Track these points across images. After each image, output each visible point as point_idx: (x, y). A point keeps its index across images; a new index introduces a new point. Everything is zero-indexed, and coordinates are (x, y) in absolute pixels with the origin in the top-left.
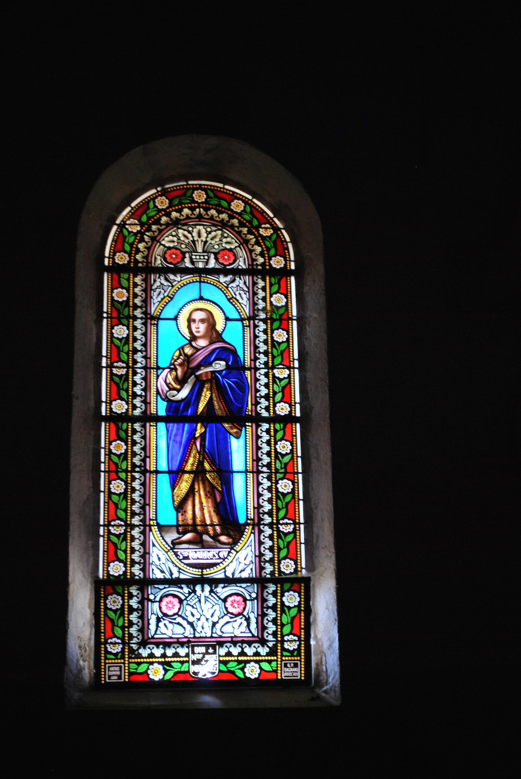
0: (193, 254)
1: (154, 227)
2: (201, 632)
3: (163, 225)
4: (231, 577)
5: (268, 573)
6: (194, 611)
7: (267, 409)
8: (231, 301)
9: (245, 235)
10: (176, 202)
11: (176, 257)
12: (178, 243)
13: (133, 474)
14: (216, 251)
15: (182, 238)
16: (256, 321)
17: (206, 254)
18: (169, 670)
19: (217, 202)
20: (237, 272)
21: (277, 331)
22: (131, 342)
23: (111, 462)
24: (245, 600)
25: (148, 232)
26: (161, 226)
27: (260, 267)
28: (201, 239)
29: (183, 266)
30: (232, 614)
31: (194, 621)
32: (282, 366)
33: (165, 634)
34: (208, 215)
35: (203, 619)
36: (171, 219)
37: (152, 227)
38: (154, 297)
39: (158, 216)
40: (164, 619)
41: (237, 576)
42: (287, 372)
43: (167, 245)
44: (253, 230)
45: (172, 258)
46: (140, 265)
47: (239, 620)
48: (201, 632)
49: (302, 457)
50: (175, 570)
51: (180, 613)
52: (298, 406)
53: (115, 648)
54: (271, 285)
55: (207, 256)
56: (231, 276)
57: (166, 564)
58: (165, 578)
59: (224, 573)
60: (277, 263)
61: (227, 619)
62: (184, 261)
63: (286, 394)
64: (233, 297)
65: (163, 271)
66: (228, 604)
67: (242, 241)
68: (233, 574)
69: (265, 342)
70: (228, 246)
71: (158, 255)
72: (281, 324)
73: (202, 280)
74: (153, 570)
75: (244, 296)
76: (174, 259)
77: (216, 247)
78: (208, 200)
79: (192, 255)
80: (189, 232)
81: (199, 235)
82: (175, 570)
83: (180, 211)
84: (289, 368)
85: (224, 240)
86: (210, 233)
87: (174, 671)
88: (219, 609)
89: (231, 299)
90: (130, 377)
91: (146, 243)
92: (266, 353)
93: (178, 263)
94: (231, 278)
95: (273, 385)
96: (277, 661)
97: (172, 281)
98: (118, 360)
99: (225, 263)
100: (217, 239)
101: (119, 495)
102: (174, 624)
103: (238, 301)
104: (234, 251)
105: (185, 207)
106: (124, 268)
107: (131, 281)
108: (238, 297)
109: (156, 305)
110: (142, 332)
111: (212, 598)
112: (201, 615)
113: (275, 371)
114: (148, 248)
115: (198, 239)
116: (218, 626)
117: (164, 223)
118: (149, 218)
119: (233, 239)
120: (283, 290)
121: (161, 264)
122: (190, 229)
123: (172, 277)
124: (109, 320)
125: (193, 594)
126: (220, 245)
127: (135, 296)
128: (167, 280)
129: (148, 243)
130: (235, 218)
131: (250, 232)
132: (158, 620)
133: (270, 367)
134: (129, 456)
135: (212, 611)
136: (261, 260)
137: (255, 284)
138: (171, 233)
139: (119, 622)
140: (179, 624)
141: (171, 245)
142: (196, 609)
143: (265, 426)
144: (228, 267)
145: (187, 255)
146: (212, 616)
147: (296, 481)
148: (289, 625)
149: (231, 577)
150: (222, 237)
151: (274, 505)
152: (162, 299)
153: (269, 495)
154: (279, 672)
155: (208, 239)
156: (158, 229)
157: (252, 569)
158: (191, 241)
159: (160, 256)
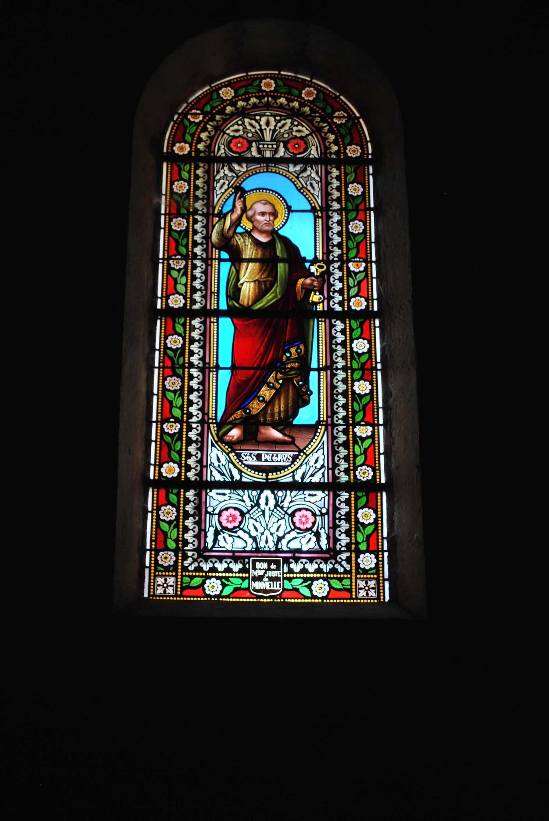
0: (260, 143)
1: (218, 117)
2: (265, 547)
3: (228, 114)
4: (300, 481)
5: (336, 256)
6: (258, 525)
7: (341, 303)
8: (302, 191)
9: (317, 124)
10: (242, 91)
11: (242, 146)
12: (244, 132)
13: (196, 217)
14: (286, 140)
15: (249, 127)
16: (330, 213)
17: (275, 143)
18: (228, 585)
19: (287, 91)
20: (308, 162)
21: (360, 468)
22: (191, 235)
23: (159, 531)
24: (314, 515)
25: (212, 122)
26: (226, 116)
27: (334, 156)
28: (269, 127)
29: (249, 155)
30: (299, 529)
31: (257, 535)
32: (358, 259)
33: (224, 547)
34: (277, 104)
35: (267, 533)
36: (237, 109)
37: (216, 117)
38: (217, 188)
39: (222, 106)
40: (224, 533)
41: (307, 480)
42: (370, 429)
43: (232, 134)
44: (327, 117)
45: (237, 147)
46: (202, 155)
47: (308, 535)
48: (265, 547)
49: (383, 408)
50: (235, 472)
51: (241, 527)
52: (375, 302)
53: (168, 510)
54: (346, 175)
55: (276, 144)
56: (302, 165)
57: (227, 466)
58: (225, 480)
59: (292, 477)
60: (353, 151)
61: (294, 534)
62: (250, 150)
63: (368, 457)
64: (303, 186)
65: (227, 161)
66: (296, 519)
67: (314, 129)
68: (303, 478)
69: (340, 234)
70: (298, 135)
71: (221, 144)
72: (363, 374)
73: (270, 170)
74: (211, 472)
75: (315, 185)
76: (240, 148)
77: (286, 136)
78: (278, 88)
79: (259, 144)
80: (257, 121)
81: (268, 123)
82: (235, 472)
83: (247, 100)
84: (373, 425)
85: (295, 128)
86: (279, 121)
87: (234, 587)
88: (285, 525)
89: (301, 189)
90: (184, 433)
91: (209, 132)
92: (340, 245)
93: (243, 152)
94: (301, 168)
95: (354, 446)
96: (351, 578)
97: (237, 172)
98: (173, 332)
99: (295, 152)
100: (287, 128)
101: (175, 392)
102: (234, 537)
103: (309, 191)
104: (305, 139)
105: (253, 97)
106: (186, 159)
107: (182, 496)
108: (309, 188)
109: (219, 196)
110: (199, 381)
111: (278, 512)
112: (265, 530)
113: (350, 265)
114: (211, 138)
115: (266, 127)
116: (284, 542)
117: (230, 113)
118: (213, 108)
119: (304, 126)
120: (366, 335)
121: (225, 153)
122: (258, 118)
123: (236, 167)
124: (161, 369)
125: (256, 508)
126: (290, 134)
127: (196, 188)
128: (231, 170)
129: (211, 132)
130: (307, 105)
131: (323, 120)
132: (217, 533)
133: (343, 260)
134: (186, 392)
135: (276, 525)
136: (335, 148)
137: (328, 173)
138: (237, 122)
139: (183, 241)
140: (239, 537)
141: (237, 134)
142: (260, 522)
143: (345, 495)
144: (298, 156)
145: (254, 144)
146: (277, 530)
147: (377, 468)
148: (362, 412)
149: (300, 481)
150: (291, 125)
151: (348, 325)
152: (226, 190)
153: (339, 229)
154: (354, 590)
155: (277, 128)
156: (223, 119)
157: (323, 474)
158: (258, 129)
159: (224, 144)
